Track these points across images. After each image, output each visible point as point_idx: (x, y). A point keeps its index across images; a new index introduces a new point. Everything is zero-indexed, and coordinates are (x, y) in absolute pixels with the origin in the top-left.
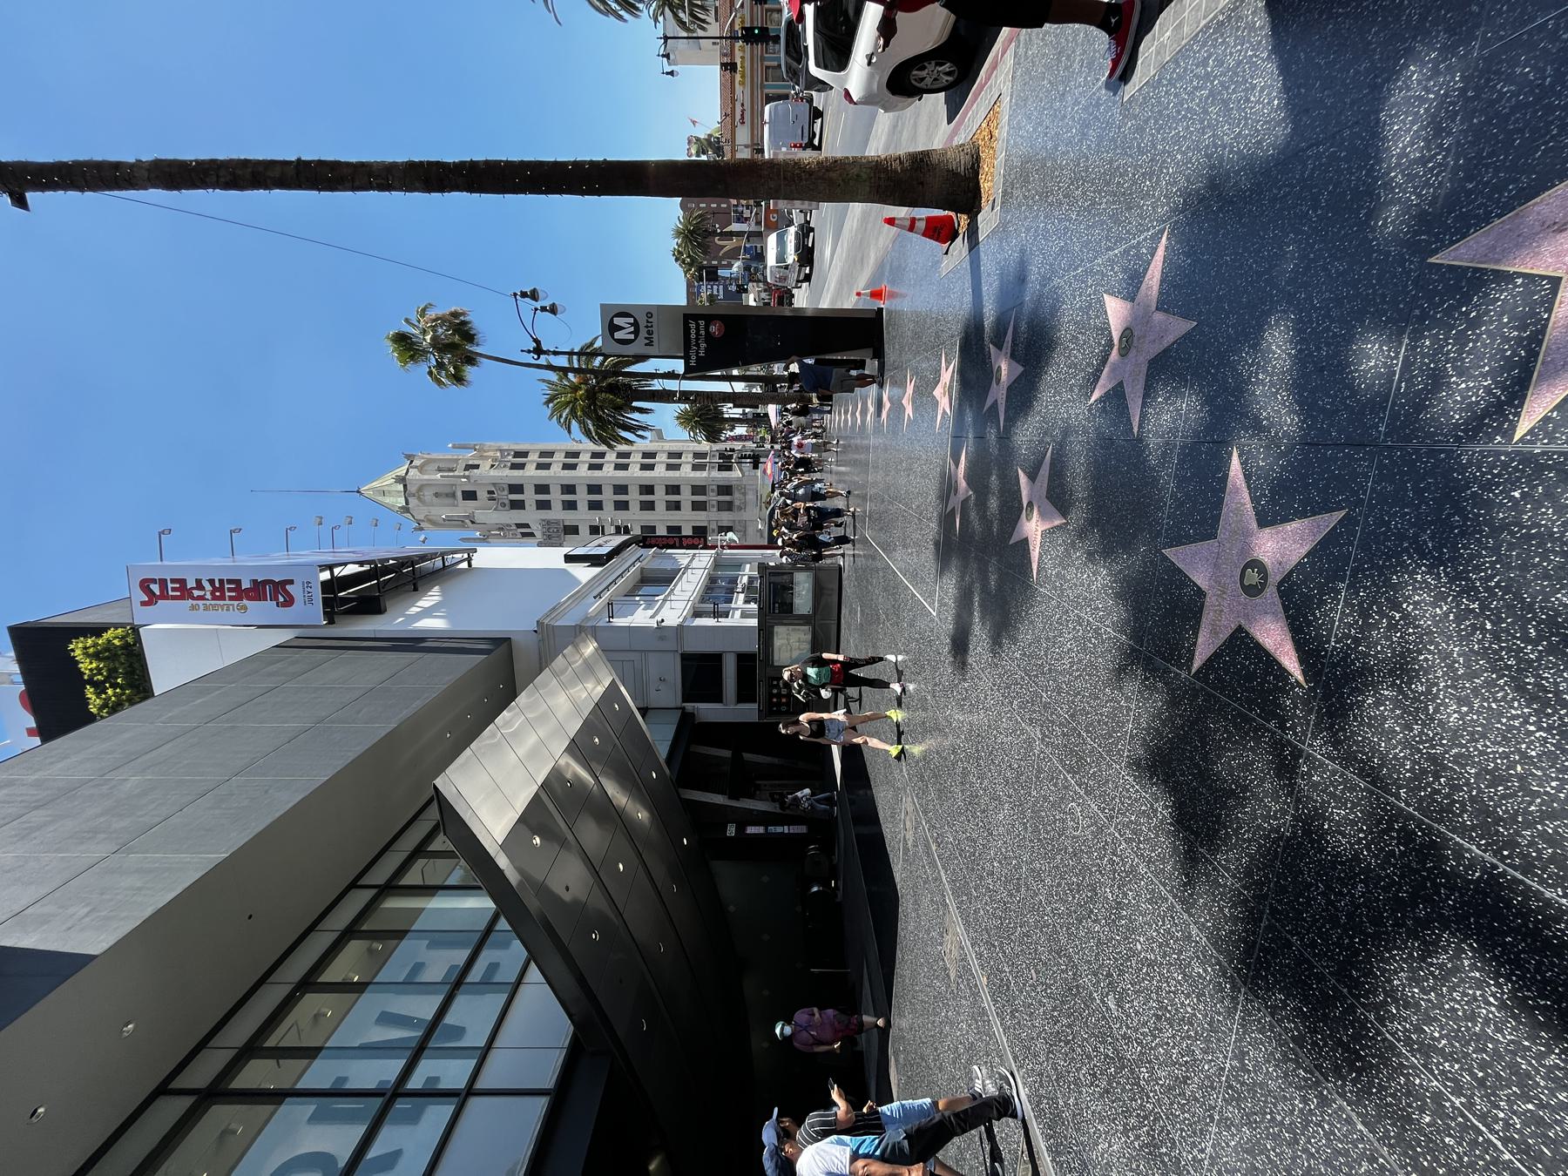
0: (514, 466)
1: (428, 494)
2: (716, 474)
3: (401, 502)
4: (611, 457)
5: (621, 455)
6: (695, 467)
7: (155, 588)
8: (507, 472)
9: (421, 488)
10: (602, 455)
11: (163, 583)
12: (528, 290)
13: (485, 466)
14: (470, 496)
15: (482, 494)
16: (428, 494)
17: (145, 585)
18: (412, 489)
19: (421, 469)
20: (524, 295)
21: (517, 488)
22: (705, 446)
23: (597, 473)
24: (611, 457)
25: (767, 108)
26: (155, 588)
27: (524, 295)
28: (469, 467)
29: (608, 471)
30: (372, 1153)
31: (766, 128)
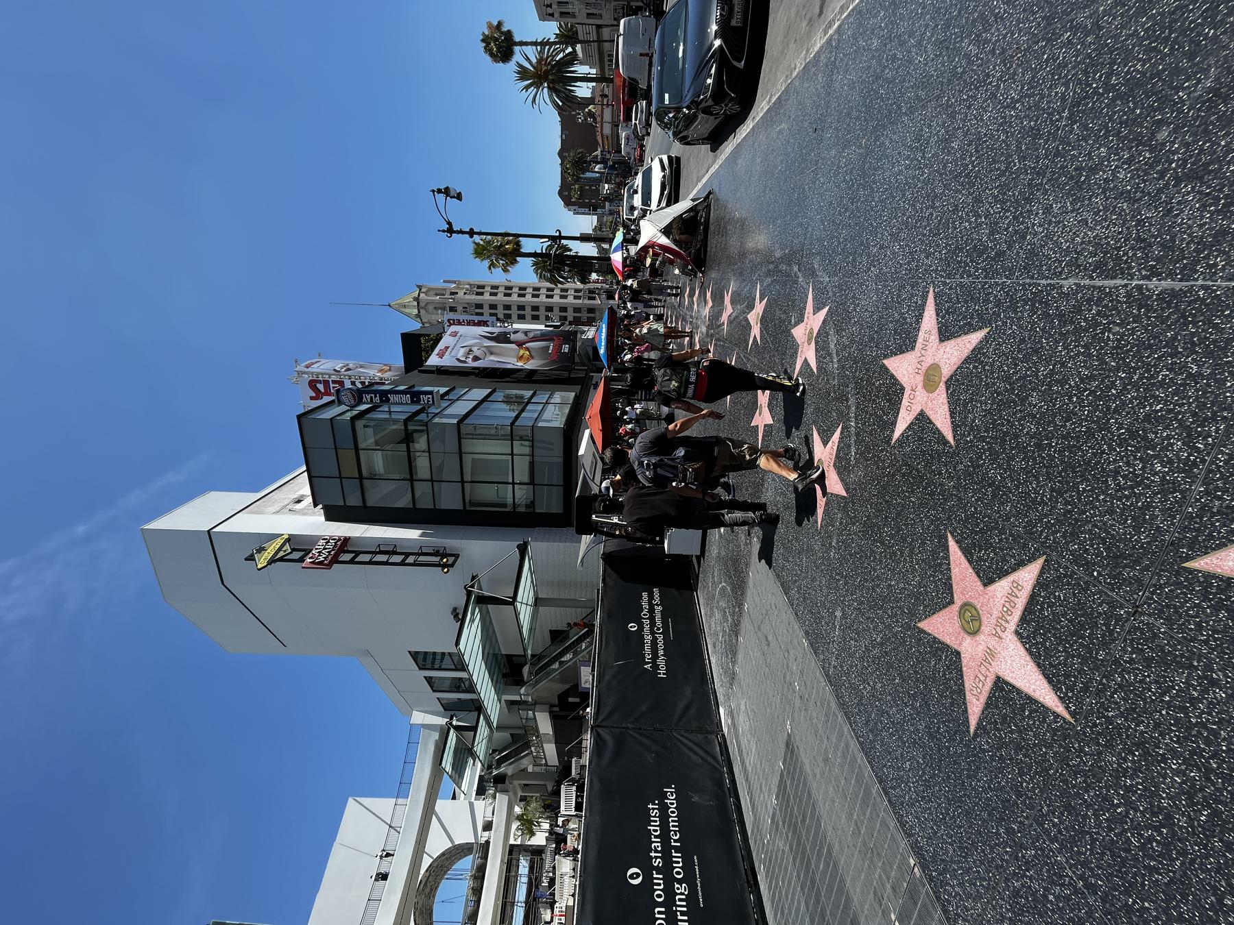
0: (478, 294)
1: (430, 308)
2: (587, 301)
3: (415, 311)
4: (557, 291)
5: (562, 290)
6: (576, 297)
7: (321, 387)
8: (474, 297)
9: (427, 304)
10: (552, 290)
11: (326, 383)
12: (442, 187)
13: (461, 294)
14: (453, 309)
15: (460, 308)
16: (430, 308)
17: (312, 384)
18: (422, 304)
19: (426, 293)
20: (439, 191)
21: (480, 306)
22: (579, 285)
23: (522, 299)
24: (557, 291)
25: (622, 22)
26: (321, 387)
27: (439, 191)
28: (452, 293)
29: (556, 299)
30: (369, 416)
31: (621, 39)
